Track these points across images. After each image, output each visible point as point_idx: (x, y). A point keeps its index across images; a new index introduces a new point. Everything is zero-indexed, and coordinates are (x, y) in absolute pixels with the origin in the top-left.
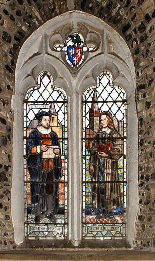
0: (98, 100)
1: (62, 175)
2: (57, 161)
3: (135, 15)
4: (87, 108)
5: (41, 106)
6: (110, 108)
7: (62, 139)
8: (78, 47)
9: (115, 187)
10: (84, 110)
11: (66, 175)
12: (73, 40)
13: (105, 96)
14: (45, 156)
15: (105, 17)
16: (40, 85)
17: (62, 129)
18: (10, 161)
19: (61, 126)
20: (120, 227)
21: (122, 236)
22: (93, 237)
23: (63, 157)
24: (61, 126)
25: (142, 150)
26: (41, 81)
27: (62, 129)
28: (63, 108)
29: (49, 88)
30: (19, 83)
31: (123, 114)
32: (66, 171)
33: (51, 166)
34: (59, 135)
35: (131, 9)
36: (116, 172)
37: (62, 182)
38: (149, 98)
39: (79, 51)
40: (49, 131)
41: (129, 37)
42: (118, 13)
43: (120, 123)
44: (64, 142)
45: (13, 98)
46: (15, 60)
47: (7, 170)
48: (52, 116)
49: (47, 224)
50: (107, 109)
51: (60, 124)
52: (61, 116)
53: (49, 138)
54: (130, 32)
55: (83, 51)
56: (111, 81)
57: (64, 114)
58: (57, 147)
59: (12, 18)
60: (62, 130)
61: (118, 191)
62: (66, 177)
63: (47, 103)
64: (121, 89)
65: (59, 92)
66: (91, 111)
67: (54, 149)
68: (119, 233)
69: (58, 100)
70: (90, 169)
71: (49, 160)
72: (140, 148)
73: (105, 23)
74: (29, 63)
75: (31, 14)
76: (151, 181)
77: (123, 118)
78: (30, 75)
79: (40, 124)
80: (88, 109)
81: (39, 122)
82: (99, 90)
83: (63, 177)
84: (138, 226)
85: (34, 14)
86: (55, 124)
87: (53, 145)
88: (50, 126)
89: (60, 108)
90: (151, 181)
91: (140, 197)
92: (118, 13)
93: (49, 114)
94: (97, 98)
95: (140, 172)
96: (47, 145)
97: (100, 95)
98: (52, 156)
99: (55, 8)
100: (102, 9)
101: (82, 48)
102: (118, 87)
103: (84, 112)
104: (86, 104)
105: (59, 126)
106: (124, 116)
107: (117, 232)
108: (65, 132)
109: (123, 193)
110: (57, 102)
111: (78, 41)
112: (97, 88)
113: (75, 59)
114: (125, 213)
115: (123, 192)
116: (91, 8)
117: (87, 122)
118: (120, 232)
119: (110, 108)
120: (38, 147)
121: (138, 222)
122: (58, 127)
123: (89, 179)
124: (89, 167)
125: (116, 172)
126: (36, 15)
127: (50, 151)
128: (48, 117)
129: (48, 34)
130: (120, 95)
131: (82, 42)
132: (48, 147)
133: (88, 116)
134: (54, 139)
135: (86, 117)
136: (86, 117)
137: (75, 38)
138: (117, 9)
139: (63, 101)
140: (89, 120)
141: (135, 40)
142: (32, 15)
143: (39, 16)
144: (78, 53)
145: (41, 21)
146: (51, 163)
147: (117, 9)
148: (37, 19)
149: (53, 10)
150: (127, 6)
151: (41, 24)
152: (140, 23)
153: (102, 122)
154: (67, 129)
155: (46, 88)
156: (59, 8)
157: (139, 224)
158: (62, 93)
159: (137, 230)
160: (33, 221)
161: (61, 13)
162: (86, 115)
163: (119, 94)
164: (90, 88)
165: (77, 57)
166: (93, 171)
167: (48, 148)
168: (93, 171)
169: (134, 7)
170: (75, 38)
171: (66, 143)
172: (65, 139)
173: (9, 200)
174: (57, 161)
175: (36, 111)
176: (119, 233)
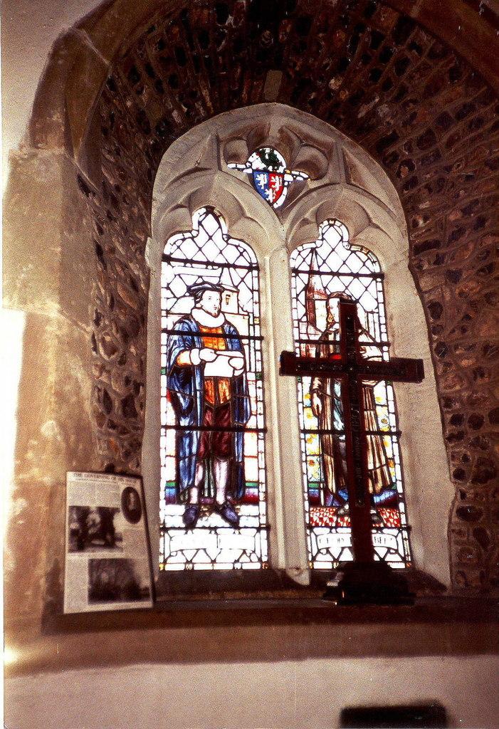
0: (322, 269)
1: (251, 414)
2: (237, 384)
3: (413, 116)
4: (300, 282)
5: (199, 270)
6: (347, 288)
7: (249, 338)
8: (274, 174)
9: (372, 443)
10: (293, 286)
11: (260, 414)
12: (264, 160)
13: (334, 264)
14: (210, 371)
15: (339, 120)
16: (198, 231)
17: (249, 319)
18: (142, 373)
19: (246, 313)
20: (396, 537)
21: (404, 560)
22: (333, 562)
23: (251, 376)
24: (246, 313)
25: (447, 365)
26: (200, 223)
27: (249, 319)
28: (248, 280)
29: (218, 237)
30: (159, 218)
31: (377, 300)
32: (260, 405)
33: (224, 394)
34: (243, 331)
35: (406, 104)
36: (372, 413)
37: (251, 430)
38: (452, 264)
39: (277, 180)
40: (219, 321)
41: (391, 158)
42: (373, 113)
43: (370, 315)
44: (252, 345)
45: (148, 242)
46: (153, 172)
47: (137, 391)
48: (226, 293)
49: (215, 528)
50: (341, 288)
51: (242, 309)
52: (245, 294)
53: (218, 336)
54: (399, 147)
55: (284, 181)
56: (346, 238)
57: (252, 291)
58: (238, 354)
59: (158, 85)
60: (249, 322)
61: (382, 453)
62: (261, 418)
63: (214, 267)
64: (366, 255)
65: (239, 248)
66: (308, 288)
67: (232, 358)
68: (394, 552)
69: (237, 263)
70: (312, 403)
71: (217, 380)
72: (439, 361)
73: (338, 132)
74: (184, 183)
75: (194, 90)
76: (488, 428)
77: (378, 307)
78: (185, 207)
79: (198, 305)
80: (301, 286)
81: (196, 303)
82: (323, 251)
83: (253, 418)
84: (460, 533)
85: (200, 91)
86: (232, 307)
87: (227, 349)
88: (220, 311)
89: (243, 280)
90: (488, 428)
91: (454, 465)
92: (373, 113)
93: (218, 288)
94: (319, 267)
95: (445, 410)
96: (216, 350)
97: (324, 262)
98: (228, 373)
99: (241, 89)
100: (337, 104)
101: (282, 175)
102: (362, 249)
103: (293, 291)
104: (297, 275)
105: (241, 312)
106: (378, 303)
107: (389, 549)
108: (254, 325)
109: (393, 459)
110: (235, 266)
111: (273, 161)
112: (317, 247)
113: (269, 192)
114: (401, 506)
115: (394, 456)
116: (313, 103)
117: (302, 311)
118: (397, 551)
119: (347, 288)
120: (195, 351)
121: (456, 524)
122: (238, 314)
123: (312, 423)
124: (311, 399)
125: (372, 413)
126: (204, 93)
127: (222, 360)
128: (216, 295)
129: (221, 137)
130: (366, 264)
131: (281, 164)
132: (218, 352)
133: (302, 297)
134: (231, 338)
135: (297, 300)
136: (297, 300)
137: (267, 157)
138: (371, 105)
139: (248, 265)
140: (305, 306)
141: (408, 163)
142: (196, 92)
143: (208, 99)
144: (274, 184)
145: (210, 109)
146: (224, 388)
147: (371, 105)
148: (204, 104)
149: (237, 94)
150: (396, 99)
151: (209, 116)
152: (422, 132)
153: (331, 310)
154: (258, 319)
155: (210, 238)
156: (249, 93)
157: (464, 529)
158: (245, 250)
159: (457, 543)
160: (180, 522)
161: (249, 103)
162: (298, 295)
163: (364, 263)
164: (304, 246)
165: (274, 189)
166: (320, 409)
167: (218, 355)
168: (320, 409)
169: (414, 102)
170: (267, 157)
171: (258, 347)
172: (255, 338)
173: (138, 465)
174: (237, 384)
175: (190, 281)
176: (394, 552)
